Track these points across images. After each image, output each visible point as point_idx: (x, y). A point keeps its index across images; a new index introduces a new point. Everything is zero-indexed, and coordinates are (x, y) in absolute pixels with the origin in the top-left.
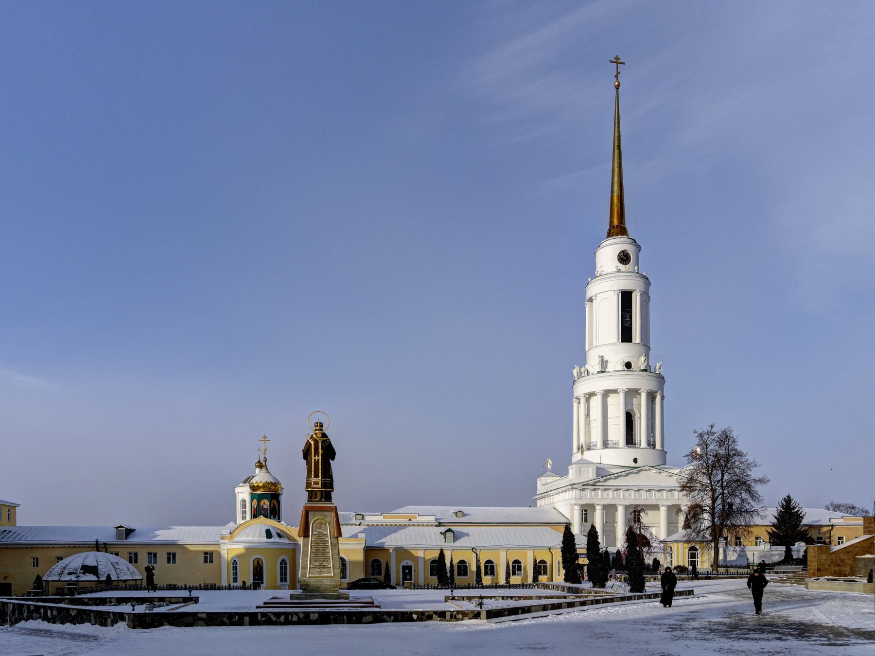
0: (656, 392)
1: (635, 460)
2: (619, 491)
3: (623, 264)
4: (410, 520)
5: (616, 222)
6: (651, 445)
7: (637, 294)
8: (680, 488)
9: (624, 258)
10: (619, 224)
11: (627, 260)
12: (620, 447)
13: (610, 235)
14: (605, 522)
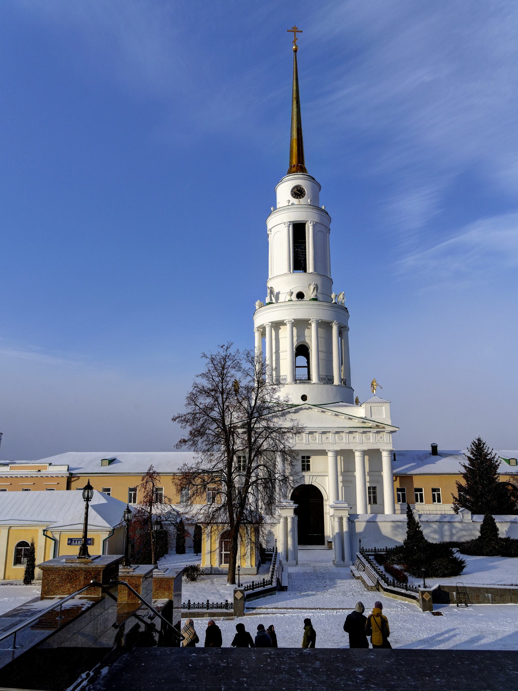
0: (332, 322)
1: (304, 398)
2: (341, 434)
3: (297, 198)
4: (39, 471)
5: (294, 162)
6: (328, 379)
7: (309, 224)
8: (185, 432)
9: (298, 192)
10: (296, 163)
11: (301, 195)
12: (287, 383)
13: (290, 172)
14: (343, 471)
